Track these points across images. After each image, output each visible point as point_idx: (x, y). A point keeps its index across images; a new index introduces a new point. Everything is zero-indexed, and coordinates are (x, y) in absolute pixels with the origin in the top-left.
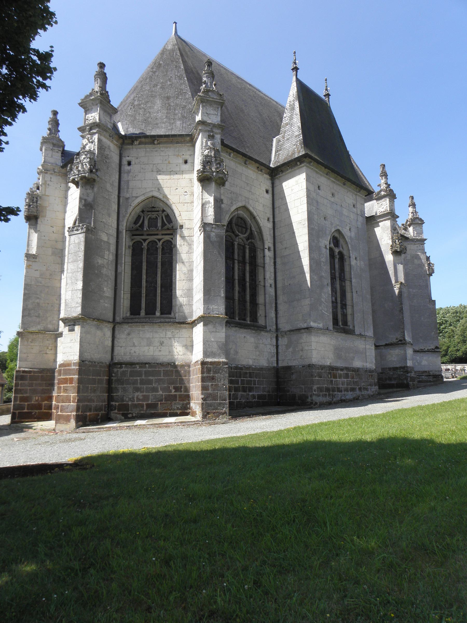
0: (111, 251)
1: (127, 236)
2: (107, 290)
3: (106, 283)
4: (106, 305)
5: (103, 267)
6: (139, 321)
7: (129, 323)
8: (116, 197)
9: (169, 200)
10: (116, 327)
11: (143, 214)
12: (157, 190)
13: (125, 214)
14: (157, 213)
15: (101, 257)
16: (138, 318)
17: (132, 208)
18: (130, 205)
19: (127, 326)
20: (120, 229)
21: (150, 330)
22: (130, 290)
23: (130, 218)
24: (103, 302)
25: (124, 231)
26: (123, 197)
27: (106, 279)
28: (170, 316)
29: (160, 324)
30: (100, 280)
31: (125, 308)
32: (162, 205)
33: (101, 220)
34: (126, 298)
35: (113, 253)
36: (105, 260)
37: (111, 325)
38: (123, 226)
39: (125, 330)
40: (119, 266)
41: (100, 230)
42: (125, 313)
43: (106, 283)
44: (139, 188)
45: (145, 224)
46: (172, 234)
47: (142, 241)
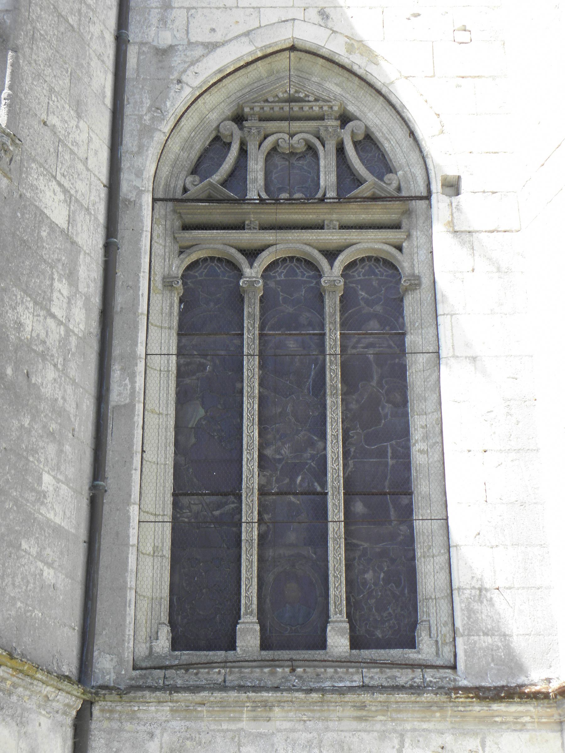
0: (82, 288)
1: (159, 230)
2: (56, 490)
3: (52, 449)
4: (49, 574)
5: (43, 356)
6: (233, 679)
7: (175, 689)
8: (110, 38)
9: (377, 64)
10: (96, 711)
11: (241, 128)
12: (316, 18)
13: (153, 119)
14: (313, 124)
15: (36, 303)
16: (224, 663)
17: (187, 94)
18: (179, 81)
19: (166, 708)
20: (125, 187)
21: (305, 736)
22: (169, 510)
23: (175, 146)
24: (34, 551)
25: (147, 199)
26: (142, 44)
27: (53, 426)
28: (411, 655)
29: (366, 697)
30: (26, 422)
31: (145, 604)
32: (338, 90)
33: (44, 117)
34: (150, 549)
35: (88, 299)
36: (50, 322)
37: (71, 700)
38: (139, 174)
39: (152, 735)
40: (116, 374)
41: (34, 160)
42: (143, 633)
43: (52, 449)
44: (225, 7)
45: (250, 176)
46: (397, 226)
47: (241, 259)
